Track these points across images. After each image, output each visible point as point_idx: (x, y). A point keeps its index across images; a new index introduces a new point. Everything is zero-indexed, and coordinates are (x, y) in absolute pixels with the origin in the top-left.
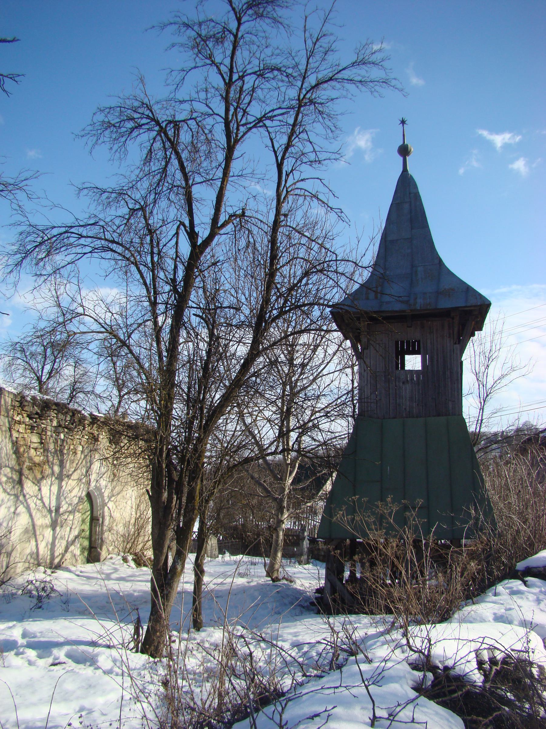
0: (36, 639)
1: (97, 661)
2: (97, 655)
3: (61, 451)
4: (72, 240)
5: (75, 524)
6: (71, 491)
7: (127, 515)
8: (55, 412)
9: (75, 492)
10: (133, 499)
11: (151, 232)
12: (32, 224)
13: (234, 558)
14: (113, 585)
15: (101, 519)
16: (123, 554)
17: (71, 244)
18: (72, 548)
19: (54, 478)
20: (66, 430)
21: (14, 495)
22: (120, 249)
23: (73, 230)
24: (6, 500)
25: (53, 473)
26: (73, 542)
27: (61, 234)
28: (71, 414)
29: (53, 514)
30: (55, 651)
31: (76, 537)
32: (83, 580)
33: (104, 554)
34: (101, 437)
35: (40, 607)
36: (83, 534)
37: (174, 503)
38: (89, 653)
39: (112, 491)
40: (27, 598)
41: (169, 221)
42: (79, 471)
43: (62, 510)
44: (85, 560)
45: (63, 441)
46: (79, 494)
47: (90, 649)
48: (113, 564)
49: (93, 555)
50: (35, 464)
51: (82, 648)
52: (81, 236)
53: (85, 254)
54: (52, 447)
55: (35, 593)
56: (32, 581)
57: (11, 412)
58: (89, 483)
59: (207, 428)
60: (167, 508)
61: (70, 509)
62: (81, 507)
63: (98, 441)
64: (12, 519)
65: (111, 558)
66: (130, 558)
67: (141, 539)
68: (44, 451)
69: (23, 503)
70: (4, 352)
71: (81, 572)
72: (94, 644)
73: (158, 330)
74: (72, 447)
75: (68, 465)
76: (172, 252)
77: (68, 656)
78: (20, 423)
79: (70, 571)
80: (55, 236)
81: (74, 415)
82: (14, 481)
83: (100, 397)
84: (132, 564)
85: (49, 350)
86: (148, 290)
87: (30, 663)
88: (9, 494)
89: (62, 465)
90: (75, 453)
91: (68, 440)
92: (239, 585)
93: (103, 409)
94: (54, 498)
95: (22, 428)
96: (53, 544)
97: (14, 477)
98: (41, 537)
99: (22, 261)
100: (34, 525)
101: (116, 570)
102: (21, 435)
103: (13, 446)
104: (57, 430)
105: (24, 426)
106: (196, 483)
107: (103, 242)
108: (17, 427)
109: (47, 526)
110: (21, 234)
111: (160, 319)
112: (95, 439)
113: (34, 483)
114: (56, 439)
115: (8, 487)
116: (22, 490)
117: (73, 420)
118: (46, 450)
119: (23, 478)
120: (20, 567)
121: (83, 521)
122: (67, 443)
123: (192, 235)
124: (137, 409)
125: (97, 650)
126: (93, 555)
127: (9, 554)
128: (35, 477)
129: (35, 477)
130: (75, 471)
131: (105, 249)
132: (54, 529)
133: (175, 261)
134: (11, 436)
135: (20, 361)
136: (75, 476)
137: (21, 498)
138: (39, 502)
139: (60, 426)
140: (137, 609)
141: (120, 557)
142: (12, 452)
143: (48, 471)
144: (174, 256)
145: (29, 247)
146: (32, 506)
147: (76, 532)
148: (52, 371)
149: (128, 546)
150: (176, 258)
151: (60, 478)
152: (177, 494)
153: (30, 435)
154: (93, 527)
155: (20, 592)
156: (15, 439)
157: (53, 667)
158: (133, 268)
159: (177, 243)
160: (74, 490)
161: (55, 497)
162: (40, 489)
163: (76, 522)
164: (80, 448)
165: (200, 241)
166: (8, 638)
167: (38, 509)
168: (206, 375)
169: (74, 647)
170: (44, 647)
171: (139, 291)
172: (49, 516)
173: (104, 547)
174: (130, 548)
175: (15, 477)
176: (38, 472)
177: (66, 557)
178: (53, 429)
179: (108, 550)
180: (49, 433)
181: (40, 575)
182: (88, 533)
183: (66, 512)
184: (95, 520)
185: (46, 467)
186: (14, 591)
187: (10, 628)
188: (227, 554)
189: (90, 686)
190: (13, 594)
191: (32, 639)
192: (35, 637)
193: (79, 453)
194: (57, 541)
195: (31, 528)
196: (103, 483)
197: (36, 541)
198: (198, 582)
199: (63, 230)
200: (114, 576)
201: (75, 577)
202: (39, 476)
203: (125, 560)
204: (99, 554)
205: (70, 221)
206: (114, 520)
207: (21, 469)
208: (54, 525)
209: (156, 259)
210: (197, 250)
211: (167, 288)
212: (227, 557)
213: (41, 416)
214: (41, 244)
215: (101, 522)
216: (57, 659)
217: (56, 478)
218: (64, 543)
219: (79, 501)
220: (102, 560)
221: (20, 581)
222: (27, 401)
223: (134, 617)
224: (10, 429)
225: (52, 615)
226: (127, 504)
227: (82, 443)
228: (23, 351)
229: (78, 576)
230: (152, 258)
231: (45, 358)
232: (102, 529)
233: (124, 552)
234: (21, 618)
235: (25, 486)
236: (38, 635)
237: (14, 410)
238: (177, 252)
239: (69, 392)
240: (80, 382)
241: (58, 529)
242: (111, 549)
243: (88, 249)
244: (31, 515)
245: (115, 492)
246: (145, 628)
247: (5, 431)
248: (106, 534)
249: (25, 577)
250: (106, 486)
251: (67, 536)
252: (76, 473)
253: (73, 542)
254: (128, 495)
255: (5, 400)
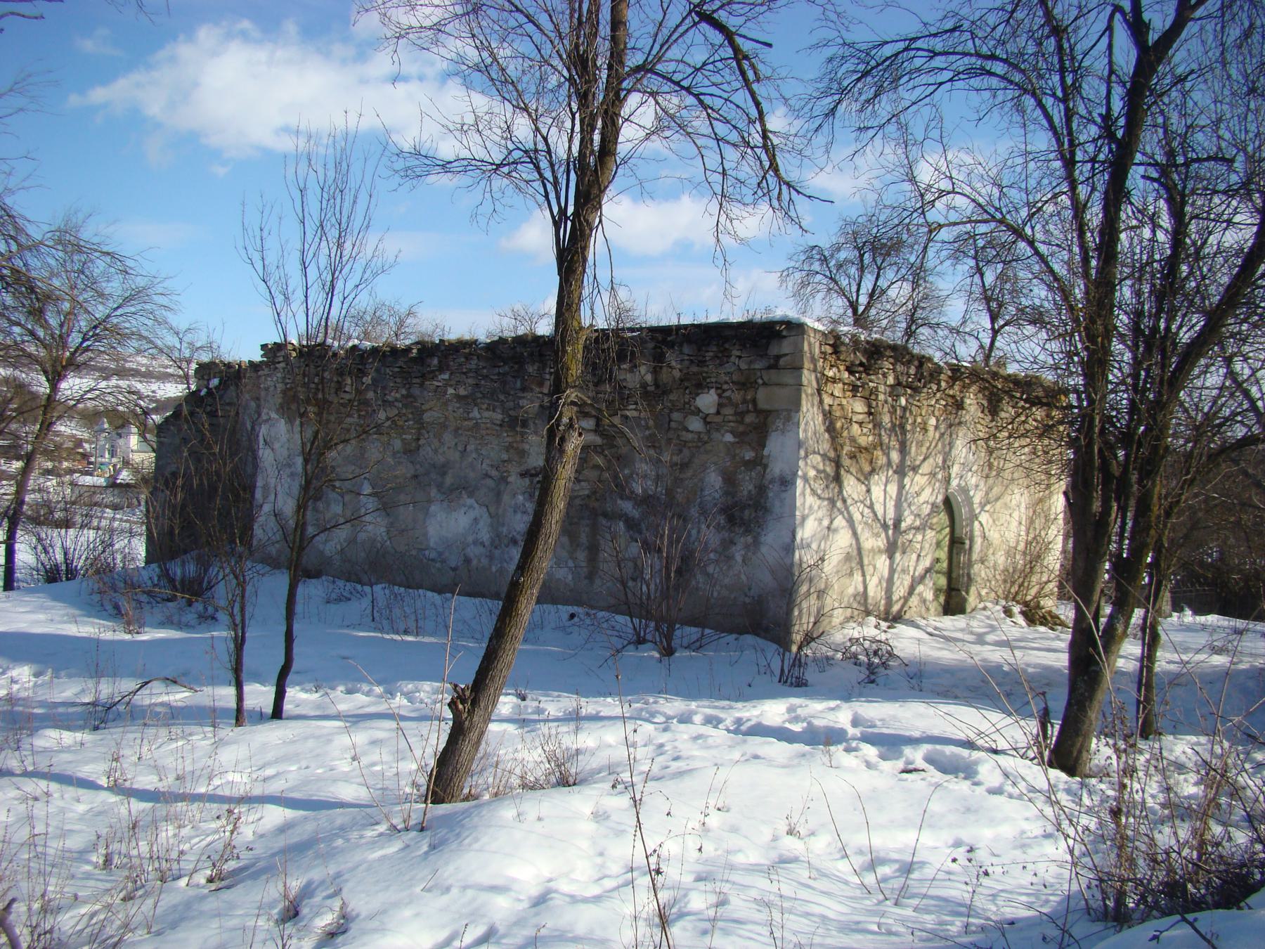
0: (875, 730)
1: (976, 773)
2: (976, 763)
3: (902, 427)
4: (918, 62)
5: (926, 549)
6: (918, 494)
7: (1011, 537)
8: (891, 360)
9: (926, 495)
10: (1023, 510)
11: (1058, 31)
12: (847, 41)
13: (1201, 619)
14: (997, 656)
15: (967, 542)
16: (1003, 602)
17: (918, 70)
18: (920, 588)
19: (890, 472)
20: (909, 391)
21: (829, 499)
22: (999, 68)
23: (919, 44)
24: (816, 507)
25: (889, 464)
26: (923, 578)
27: (896, 55)
28: (916, 363)
29: (890, 532)
30: (908, 751)
31: (928, 571)
32: (938, 642)
33: (972, 600)
34: (968, 401)
35: (873, 682)
36: (937, 567)
37: (1113, 515)
38: (963, 758)
39: (987, 494)
40: (849, 665)
41: (1090, 6)
42: (931, 460)
43: (903, 525)
44: (940, 609)
45: (904, 409)
46: (932, 500)
47: (965, 752)
48: (988, 618)
49: (953, 603)
50: (861, 449)
51: (949, 750)
52: (934, 54)
53: (941, 84)
54: (886, 419)
55: (862, 658)
56: (858, 640)
57: (820, 363)
58: (948, 480)
59: (1176, 380)
60: (1101, 525)
61: (918, 523)
62: (935, 520)
63: (963, 409)
64: (825, 538)
65: (985, 608)
66: (1016, 609)
67: (1034, 579)
68: (874, 426)
69: (842, 513)
70: (792, 264)
71: (936, 628)
72: (969, 745)
73: (1079, 209)
74: (919, 420)
75: (913, 449)
76: (1101, 66)
77: (929, 760)
78: (834, 380)
79: (918, 627)
80: (887, 59)
81: (921, 365)
82: (827, 476)
83: (958, 332)
84: (1020, 620)
85: (866, 256)
86: (1058, 141)
87: (869, 765)
88: (820, 498)
89: (903, 450)
90: (925, 430)
91: (913, 408)
92: (1217, 666)
93: (967, 352)
94: (891, 505)
95: (837, 389)
96: (890, 581)
97: (828, 469)
98: (871, 568)
99: (836, 107)
100: (859, 549)
101: (993, 629)
102: (837, 401)
103: (825, 420)
104: (894, 391)
105: (840, 385)
106: (1154, 482)
107: (973, 60)
108: (829, 387)
109: (880, 551)
110: (830, 60)
111: (1083, 191)
112: (959, 405)
113: (859, 480)
114: (893, 406)
115: (819, 487)
116: (840, 492)
117: (920, 374)
118: (877, 425)
119: (842, 472)
120: (838, 616)
121: (938, 544)
122: (911, 412)
123: (1138, 28)
124: (1030, 352)
125: (976, 755)
126: (953, 603)
127: (821, 594)
128: (861, 470)
129: (861, 470)
130: (925, 459)
131: (972, 72)
132: (891, 557)
133: (1109, 82)
134: (821, 402)
135: (819, 277)
136: (926, 468)
137: (839, 504)
138: (866, 511)
139: (899, 384)
140: (1044, 694)
141: (998, 608)
142: (822, 429)
143: (882, 460)
144: (1106, 73)
145: (845, 83)
146: (857, 517)
147: (926, 562)
148: (874, 290)
149: (1013, 590)
150: (1109, 76)
151: (901, 472)
152: (1118, 500)
153: (851, 401)
154: (955, 556)
155: (839, 656)
156: (827, 408)
157: (905, 775)
158: (1029, 102)
159: (1110, 47)
160: (924, 491)
161: (893, 503)
162: (868, 491)
163: (927, 546)
164: (933, 421)
165: (1153, 37)
166: (832, 724)
167: (866, 523)
168: (1168, 288)
169: (938, 747)
170: (890, 744)
171: (1042, 141)
172: (883, 535)
173: (973, 590)
174: (1017, 593)
175: (830, 470)
176: (865, 461)
177: (910, 603)
178: (888, 389)
179: (979, 594)
180: (881, 397)
181: (870, 629)
182: (945, 565)
183: (910, 528)
184: (957, 544)
185: (878, 453)
186: (830, 654)
187: (833, 709)
188: (1188, 612)
189: (968, 810)
190: (828, 658)
191: (870, 730)
192: (874, 726)
193: (931, 429)
194: (896, 576)
195: (855, 553)
196: (973, 480)
197: (864, 575)
198: (1148, 658)
199: (901, 45)
200: (990, 638)
201: (927, 636)
202: (867, 468)
203: (1008, 612)
204: (965, 600)
205: (912, 29)
206: (990, 545)
207: (839, 456)
208: (891, 550)
209: (1069, 81)
210: (1151, 54)
211: (1094, 131)
212: (1188, 617)
213: (867, 369)
214: (865, 74)
215: (967, 546)
216: (911, 763)
217: (895, 472)
218: (907, 581)
219: (932, 511)
220: (968, 610)
221: (839, 637)
222: (843, 343)
223: (1035, 707)
224: (819, 391)
225: (893, 694)
226: (1021, 515)
227: (937, 413)
228: (824, 260)
229: (931, 634)
230: (1062, 79)
231: (862, 269)
232: (970, 560)
233: (1006, 598)
234: (847, 698)
235: (845, 483)
236: (878, 723)
237: (825, 359)
238: (1110, 63)
239: (904, 325)
240: (923, 308)
241: (898, 556)
242: (983, 592)
243: (947, 75)
244: (855, 534)
245: (992, 495)
246: (1057, 728)
247: (812, 395)
248: (977, 568)
249: (846, 631)
250: (977, 486)
251: (911, 569)
252: (926, 464)
253: (923, 578)
254: (1014, 502)
255: (810, 344)
